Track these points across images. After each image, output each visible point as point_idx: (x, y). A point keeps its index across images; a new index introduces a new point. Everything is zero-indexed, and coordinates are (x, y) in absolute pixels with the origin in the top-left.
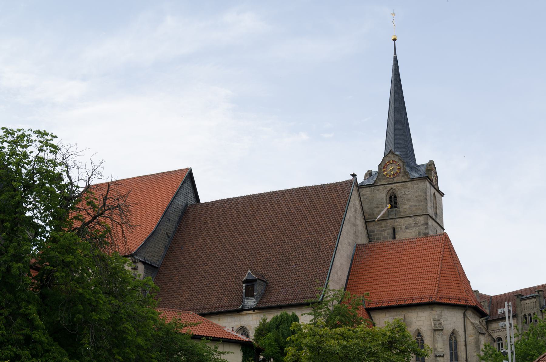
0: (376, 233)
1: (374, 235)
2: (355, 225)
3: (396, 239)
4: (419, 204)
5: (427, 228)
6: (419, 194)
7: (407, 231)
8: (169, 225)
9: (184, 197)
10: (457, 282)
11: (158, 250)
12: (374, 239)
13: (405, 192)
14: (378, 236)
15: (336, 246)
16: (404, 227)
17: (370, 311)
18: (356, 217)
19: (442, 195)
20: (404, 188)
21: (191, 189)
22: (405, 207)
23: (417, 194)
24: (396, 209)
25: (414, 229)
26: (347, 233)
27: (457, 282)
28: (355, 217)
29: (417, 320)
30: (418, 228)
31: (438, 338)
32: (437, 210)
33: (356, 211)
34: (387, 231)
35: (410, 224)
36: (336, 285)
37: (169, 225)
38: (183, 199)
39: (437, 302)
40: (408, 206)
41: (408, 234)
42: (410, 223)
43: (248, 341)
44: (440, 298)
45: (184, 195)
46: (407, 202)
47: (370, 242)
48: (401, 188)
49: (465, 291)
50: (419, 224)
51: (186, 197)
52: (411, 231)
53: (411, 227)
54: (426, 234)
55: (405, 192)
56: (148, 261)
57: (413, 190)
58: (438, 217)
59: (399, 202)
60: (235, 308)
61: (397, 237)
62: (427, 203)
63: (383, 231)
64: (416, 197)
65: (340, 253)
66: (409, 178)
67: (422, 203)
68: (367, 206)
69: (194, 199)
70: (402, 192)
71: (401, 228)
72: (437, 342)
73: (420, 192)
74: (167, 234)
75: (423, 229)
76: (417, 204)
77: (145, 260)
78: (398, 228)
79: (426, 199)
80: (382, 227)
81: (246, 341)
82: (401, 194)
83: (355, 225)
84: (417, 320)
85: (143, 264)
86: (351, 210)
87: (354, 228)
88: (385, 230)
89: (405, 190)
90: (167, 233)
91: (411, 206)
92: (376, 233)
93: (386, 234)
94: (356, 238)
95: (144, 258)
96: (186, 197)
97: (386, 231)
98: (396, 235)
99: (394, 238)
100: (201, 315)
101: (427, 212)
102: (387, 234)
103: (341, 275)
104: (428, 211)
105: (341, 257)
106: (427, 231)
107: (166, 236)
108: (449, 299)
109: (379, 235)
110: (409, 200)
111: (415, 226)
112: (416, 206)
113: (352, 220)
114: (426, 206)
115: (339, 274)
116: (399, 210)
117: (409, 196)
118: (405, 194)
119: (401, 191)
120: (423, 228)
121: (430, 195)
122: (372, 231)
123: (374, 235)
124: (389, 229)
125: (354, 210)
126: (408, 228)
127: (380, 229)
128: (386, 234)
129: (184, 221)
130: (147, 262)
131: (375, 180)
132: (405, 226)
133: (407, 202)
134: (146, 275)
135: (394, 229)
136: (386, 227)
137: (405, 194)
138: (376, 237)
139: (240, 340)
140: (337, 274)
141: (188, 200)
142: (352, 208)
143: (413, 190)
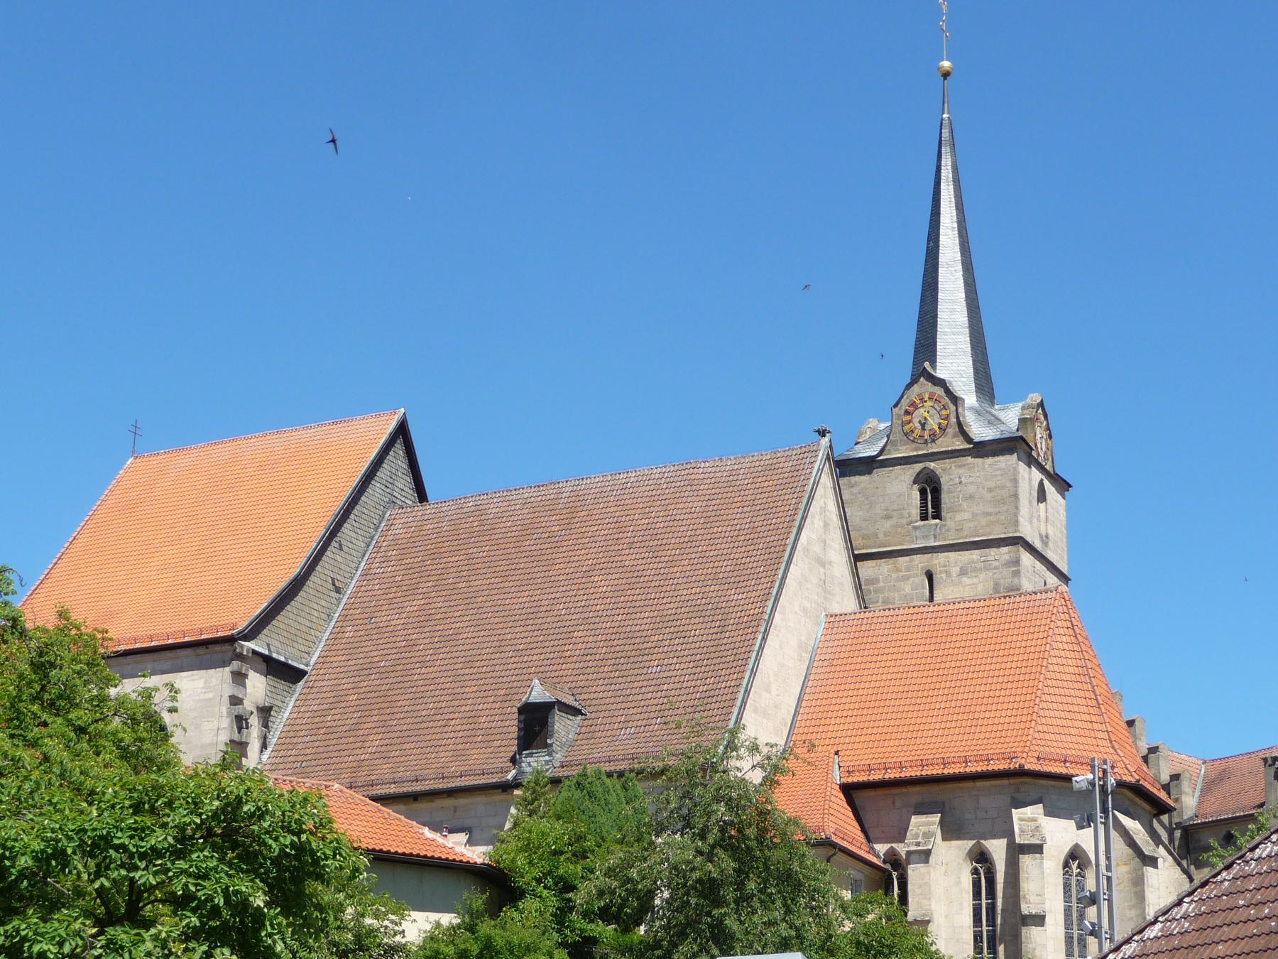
0: (882, 584)
1: (876, 591)
2: (822, 563)
3: (935, 602)
4: (997, 510)
5: (1017, 574)
6: (999, 483)
7: (965, 579)
8: (339, 559)
9: (383, 487)
10: (1088, 717)
11: (308, 624)
12: (877, 602)
13: (960, 478)
14: (886, 594)
15: (766, 617)
16: (955, 570)
17: (851, 792)
18: (828, 541)
19: (1066, 486)
20: (960, 467)
21: (405, 466)
22: (958, 517)
23: (991, 484)
24: (937, 521)
25: (982, 576)
26: (800, 584)
27: (1088, 717)
28: (825, 542)
29: (976, 818)
30: (994, 573)
31: (1030, 867)
32: (1049, 526)
33: (826, 525)
34: (911, 580)
35: (973, 562)
36: (765, 721)
37: (339, 559)
38: (381, 492)
39: (1029, 770)
40: (967, 515)
41: (967, 588)
42: (973, 559)
43: (482, 864)
44: (1038, 759)
45: (385, 483)
46: (965, 505)
47: (865, 608)
48: (951, 468)
49: (1111, 742)
50: (995, 564)
51: (390, 486)
52: (975, 580)
53: (975, 570)
54: (1014, 590)
55: (960, 478)
56: (278, 653)
57: (982, 473)
58: (1051, 544)
59: (945, 504)
60: (494, 779)
61: (938, 596)
62: (1017, 508)
63: (900, 581)
64: (990, 490)
65: (778, 636)
66: (968, 439)
67: (1005, 508)
68: (861, 513)
69: (411, 492)
70: (952, 477)
71: (948, 573)
72: (1028, 879)
73: (1000, 478)
74: (334, 585)
75: (1005, 577)
76: (991, 510)
77: (269, 650)
78: (941, 572)
79: (1016, 496)
80: (898, 570)
81: (475, 863)
82: (951, 483)
83: (822, 563)
84: (976, 818)
85: (264, 661)
86: (813, 523)
87: (822, 570)
88: (907, 578)
89: (961, 471)
90: (333, 579)
91: (974, 515)
92: (882, 584)
93: (908, 589)
94: (826, 599)
95: (268, 645)
96: (390, 486)
97: (908, 578)
98: (935, 592)
99: (931, 599)
100: (375, 799)
101: (1019, 531)
102: (912, 589)
103: (777, 695)
104: (1020, 528)
105: (781, 647)
106: (1016, 581)
107: (332, 587)
108: (1065, 762)
109: (889, 590)
110: (971, 497)
111: (986, 569)
112: (990, 514)
113: (817, 549)
114: (1016, 515)
115: (774, 691)
116: (945, 525)
117: (971, 489)
118: (960, 483)
119: (950, 474)
120: (1007, 572)
121: (1027, 485)
122: (873, 579)
123: (876, 591)
124: (916, 575)
125: (822, 524)
126: (967, 573)
127: (894, 575)
128: (908, 589)
129: (382, 549)
130: (274, 655)
131: (882, 445)
132: (958, 569)
133: (965, 505)
134: (273, 689)
135: (930, 576)
136: (908, 569)
137: (960, 483)
138: (881, 596)
139: (461, 861)
140: (769, 691)
141: (395, 494)
142: (817, 517)
143: (982, 473)
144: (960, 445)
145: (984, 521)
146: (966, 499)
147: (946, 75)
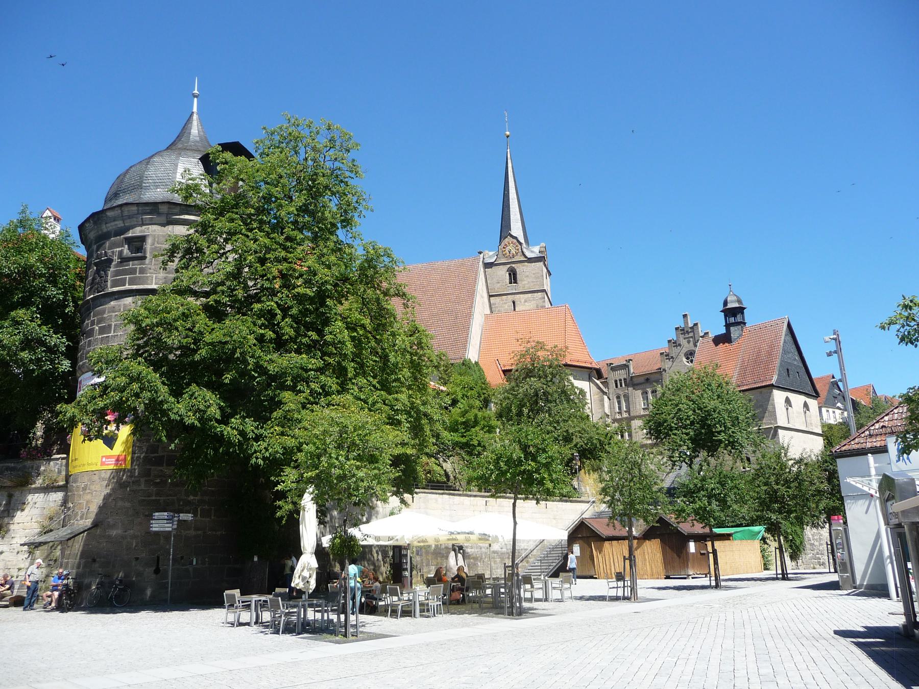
16: (523, 301)
22: (523, 283)
40: (526, 282)
64: (534, 274)
76: (264, 630)
110: (527, 276)
117: (527, 273)
144: (523, 259)
145: (532, 284)
146: (526, 277)
147: (508, 137)
